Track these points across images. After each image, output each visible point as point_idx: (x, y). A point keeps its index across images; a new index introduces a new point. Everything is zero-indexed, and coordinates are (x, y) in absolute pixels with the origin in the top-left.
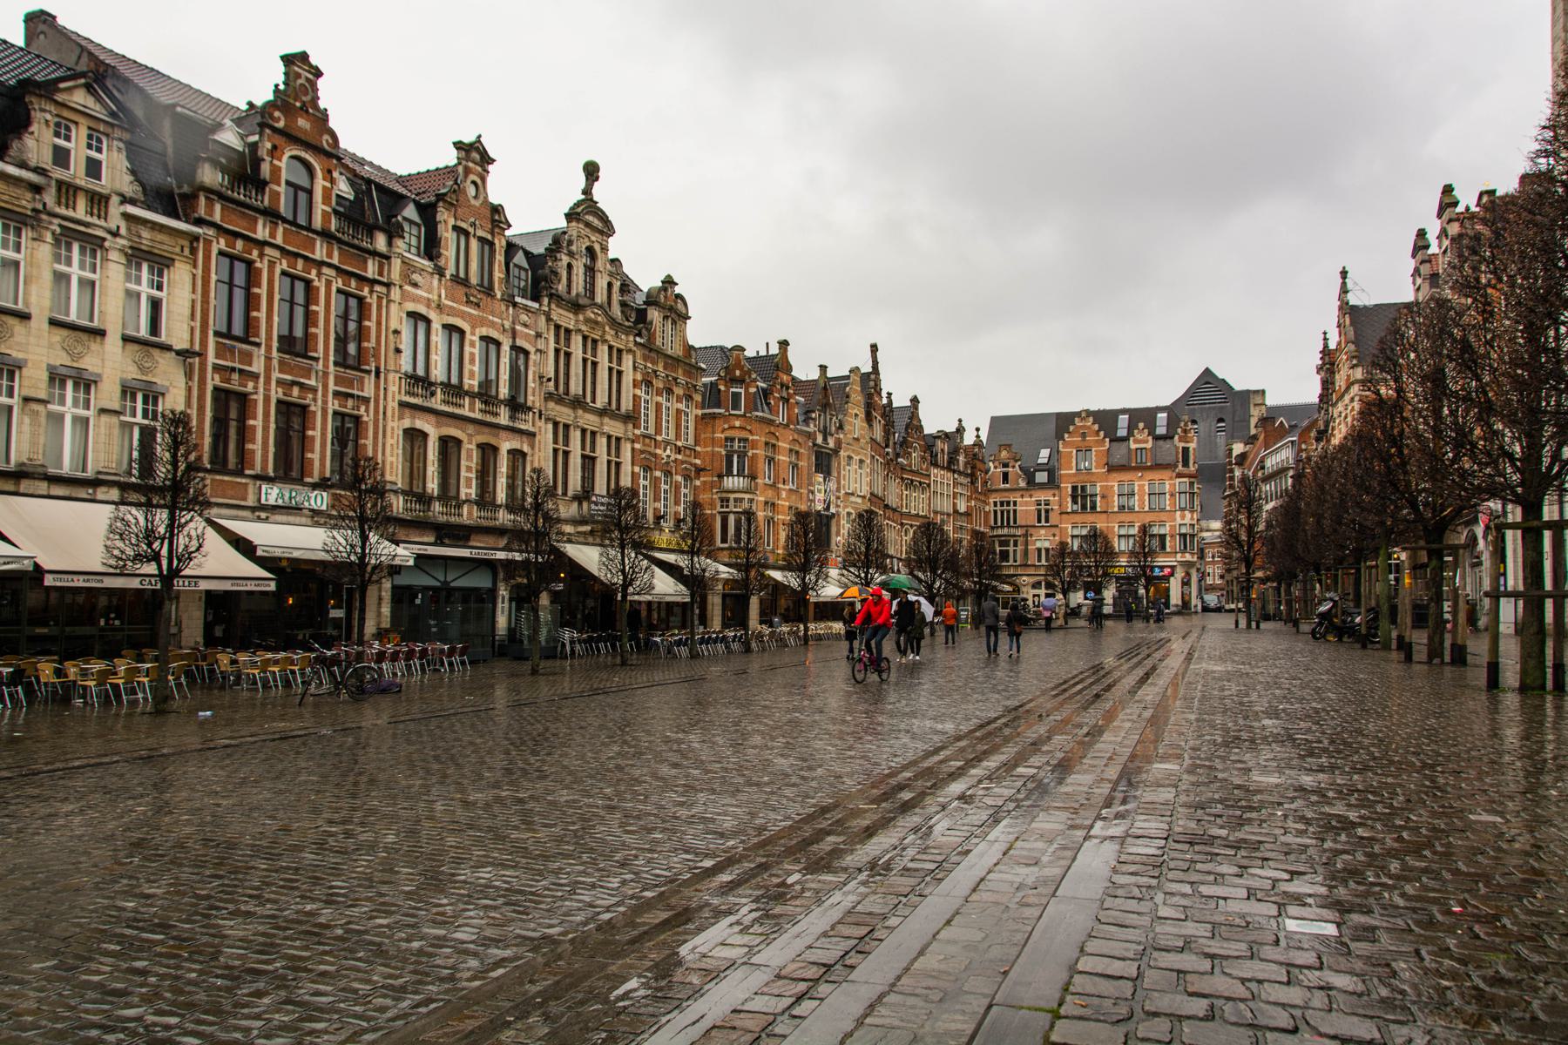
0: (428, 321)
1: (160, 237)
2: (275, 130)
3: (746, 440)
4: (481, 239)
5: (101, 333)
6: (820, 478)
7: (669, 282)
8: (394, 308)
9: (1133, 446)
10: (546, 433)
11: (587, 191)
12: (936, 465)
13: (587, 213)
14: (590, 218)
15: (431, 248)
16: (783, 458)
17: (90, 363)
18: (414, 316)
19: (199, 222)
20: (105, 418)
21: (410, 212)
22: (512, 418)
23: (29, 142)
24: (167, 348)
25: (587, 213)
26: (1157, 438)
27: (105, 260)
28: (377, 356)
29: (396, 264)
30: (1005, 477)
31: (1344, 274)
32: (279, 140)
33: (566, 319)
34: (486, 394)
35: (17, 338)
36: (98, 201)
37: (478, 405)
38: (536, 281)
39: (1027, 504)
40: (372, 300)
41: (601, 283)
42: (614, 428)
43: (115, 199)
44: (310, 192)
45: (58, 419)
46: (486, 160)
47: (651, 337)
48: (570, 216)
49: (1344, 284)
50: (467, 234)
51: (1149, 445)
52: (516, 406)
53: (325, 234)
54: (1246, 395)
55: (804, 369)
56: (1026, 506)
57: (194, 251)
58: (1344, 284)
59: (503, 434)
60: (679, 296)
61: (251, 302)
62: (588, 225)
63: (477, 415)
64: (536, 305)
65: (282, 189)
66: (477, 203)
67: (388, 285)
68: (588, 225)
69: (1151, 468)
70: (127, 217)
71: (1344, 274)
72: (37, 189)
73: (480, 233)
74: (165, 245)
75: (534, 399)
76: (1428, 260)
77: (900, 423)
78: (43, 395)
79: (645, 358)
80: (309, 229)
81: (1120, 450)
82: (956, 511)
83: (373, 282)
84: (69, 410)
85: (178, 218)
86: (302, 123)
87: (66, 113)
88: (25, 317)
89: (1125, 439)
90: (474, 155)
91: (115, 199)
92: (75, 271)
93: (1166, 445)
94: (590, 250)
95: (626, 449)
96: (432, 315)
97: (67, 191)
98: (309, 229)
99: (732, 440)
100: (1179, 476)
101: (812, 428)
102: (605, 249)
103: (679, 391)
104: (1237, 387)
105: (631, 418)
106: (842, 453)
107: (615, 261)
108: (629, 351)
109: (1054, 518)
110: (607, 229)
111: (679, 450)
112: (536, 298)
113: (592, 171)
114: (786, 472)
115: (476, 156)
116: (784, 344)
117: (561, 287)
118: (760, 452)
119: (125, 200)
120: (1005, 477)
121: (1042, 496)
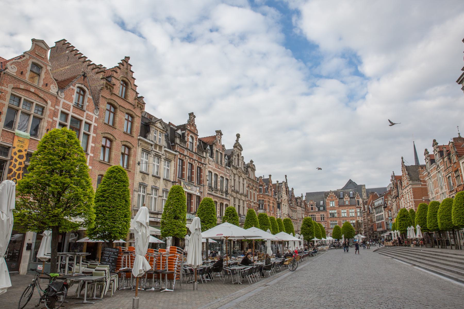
0: (211, 173)
1: (170, 155)
2: (188, 130)
3: (263, 200)
4: (221, 153)
5: (159, 178)
6: (278, 210)
7: (252, 162)
8: (207, 170)
9: (345, 200)
10: (232, 200)
11: (237, 141)
12: (297, 206)
13: (238, 146)
14: (238, 147)
15: (212, 156)
16: (271, 205)
17: (157, 185)
18: (210, 172)
19: (176, 151)
20: (160, 198)
21: (208, 147)
22: (226, 196)
23: (150, 135)
24: (170, 181)
25: (238, 146)
26: (351, 198)
27: (161, 161)
28: (203, 182)
29: (207, 159)
30: (312, 208)
31: (402, 158)
32: (189, 132)
33: (235, 171)
34: (222, 191)
35: (147, 179)
36: (160, 147)
37: (220, 193)
38: (229, 163)
39: (318, 215)
40: (203, 168)
41: (240, 162)
42: (243, 198)
43: (163, 147)
44: (192, 143)
45: (152, 198)
46: (221, 134)
47: (249, 176)
48: (234, 147)
49: (403, 161)
50: (218, 152)
51: (349, 200)
52: (227, 193)
53: (195, 153)
54: (361, 186)
55: (274, 181)
56: (318, 216)
57: (175, 158)
58: (403, 161)
59: (224, 200)
60: (254, 165)
61: (183, 169)
62: (238, 149)
63: (220, 196)
64: (229, 168)
65: (189, 143)
66: (220, 144)
67: (205, 164)
68: (238, 149)
69: (350, 206)
70: (165, 151)
71: (402, 158)
72: (152, 145)
73: (221, 151)
74: (171, 157)
75: (229, 191)
76: (430, 156)
77: (290, 194)
78: (150, 193)
79: (248, 180)
80: (192, 151)
81: (341, 201)
82: (302, 218)
83: (203, 164)
84: (153, 196)
85: (171, 149)
86: (192, 128)
87: (157, 129)
88: (148, 175)
89: (343, 198)
90: (219, 133)
91: (163, 147)
92: (156, 164)
93: (353, 200)
94: (238, 155)
95: (245, 203)
96: (213, 172)
97: (156, 145)
98: (192, 151)
99: (260, 200)
100: (357, 208)
101: (276, 197)
102: (241, 154)
103: (254, 188)
104: (358, 184)
105: (246, 196)
106: (283, 203)
107: (242, 157)
108: (246, 179)
109: (325, 219)
110: (241, 149)
111: (254, 203)
112: (229, 166)
113: (238, 136)
114: (272, 209)
115: (219, 134)
116: (270, 176)
117: (234, 164)
118: (267, 203)
119: (165, 147)
120: (312, 208)
121: (322, 213)
